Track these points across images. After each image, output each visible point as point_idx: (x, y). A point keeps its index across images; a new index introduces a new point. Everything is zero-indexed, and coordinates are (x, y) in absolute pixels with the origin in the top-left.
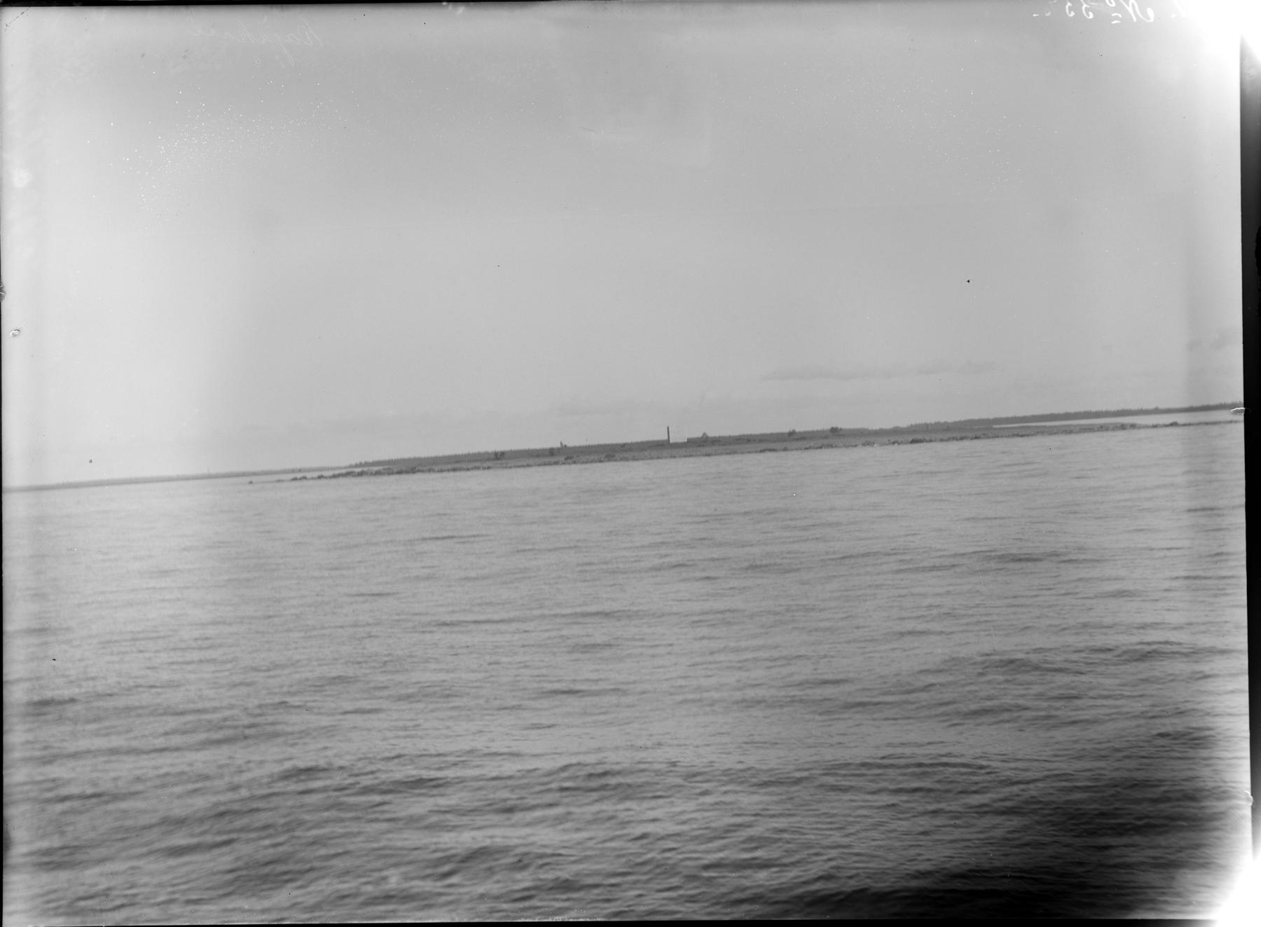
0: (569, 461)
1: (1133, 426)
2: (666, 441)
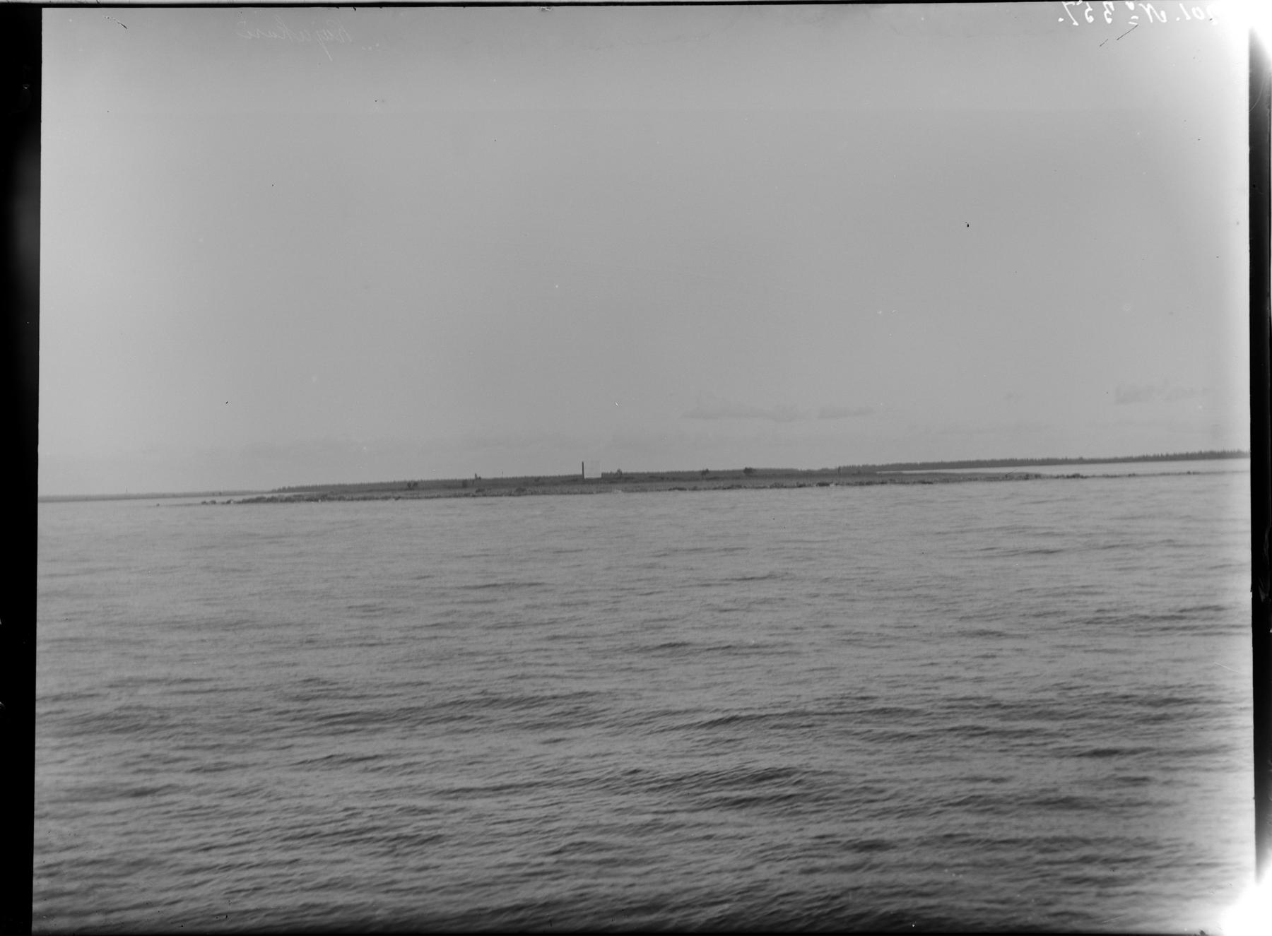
0: (480, 493)
1: (1037, 476)
2: (580, 476)
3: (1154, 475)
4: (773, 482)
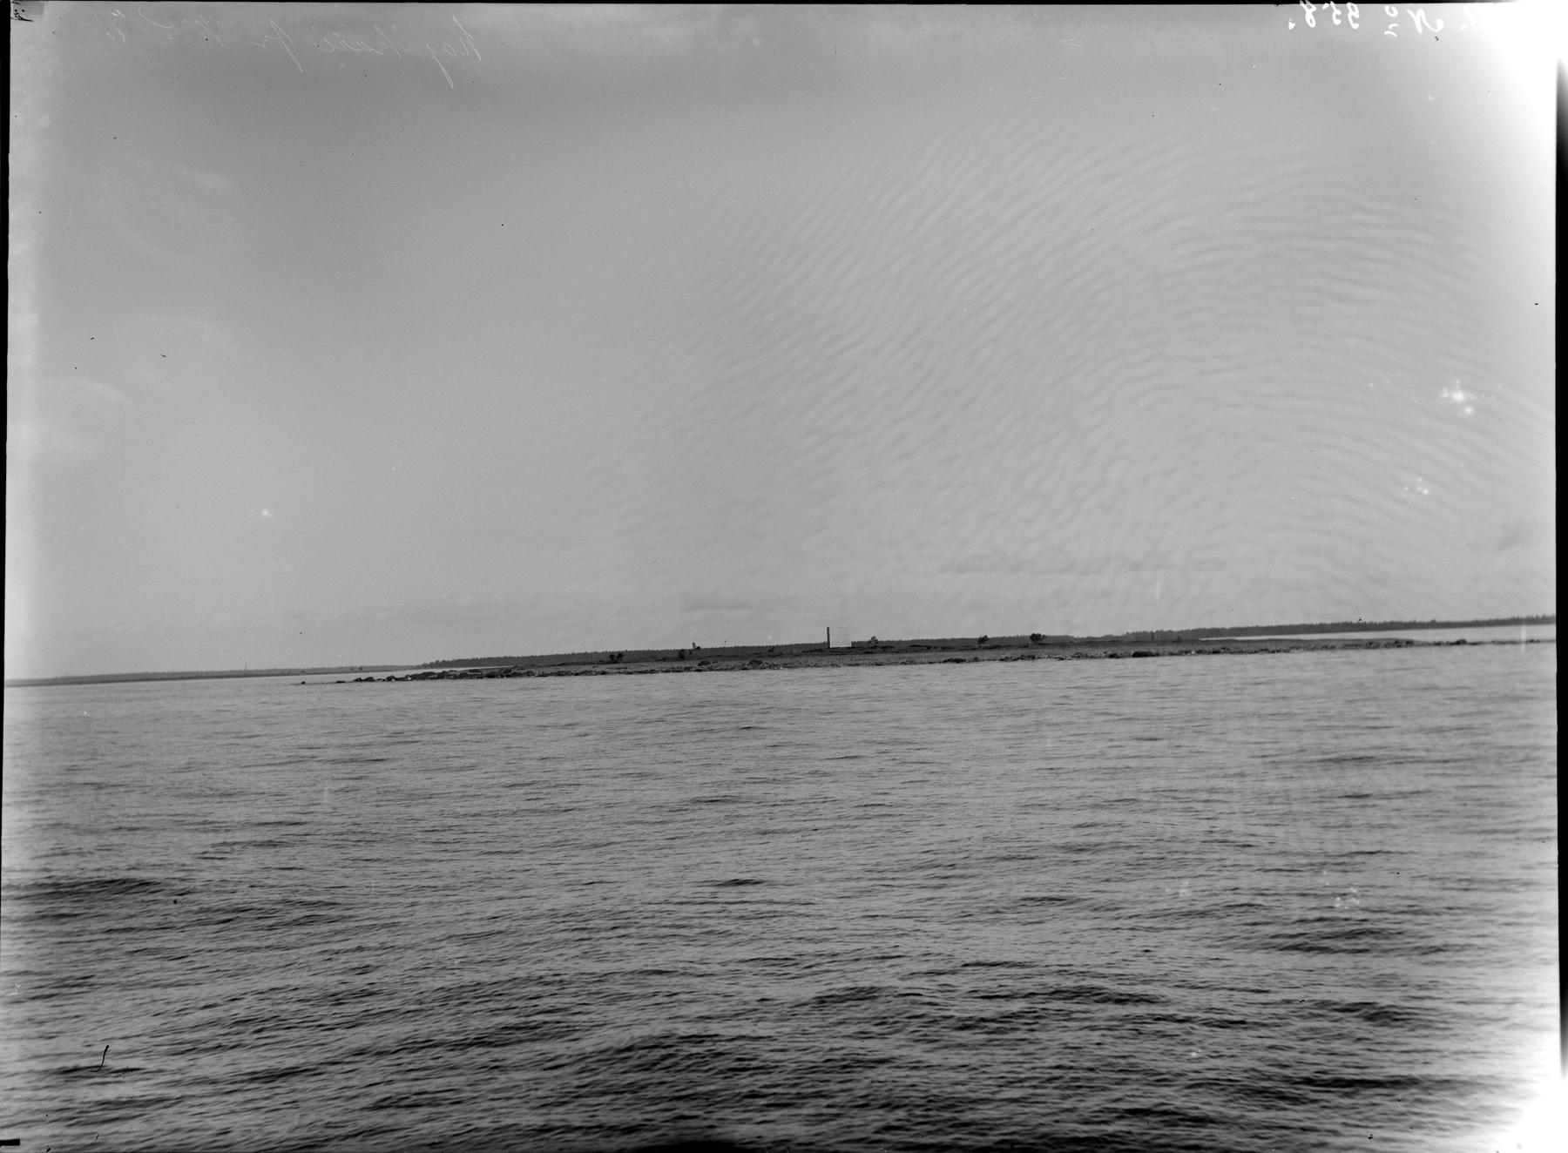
1: (1410, 643)
3: (316, 684)
4: (1074, 651)
